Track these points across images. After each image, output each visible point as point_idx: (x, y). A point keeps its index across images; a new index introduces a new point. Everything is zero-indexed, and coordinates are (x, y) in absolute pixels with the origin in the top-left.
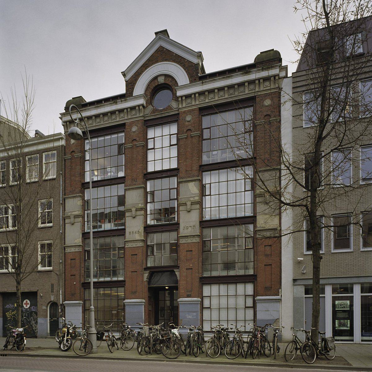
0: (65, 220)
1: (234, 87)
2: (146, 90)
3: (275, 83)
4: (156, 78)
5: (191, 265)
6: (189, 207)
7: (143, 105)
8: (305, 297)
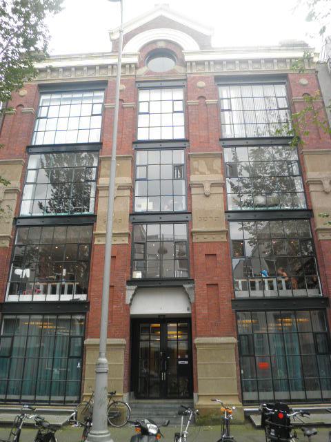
0: (190, 189)
1: (46, 71)
2: (142, 50)
3: (112, 72)
4: (155, 42)
5: (216, 278)
6: (207, 189)
7: (135, 64)
8: (108, 345)
